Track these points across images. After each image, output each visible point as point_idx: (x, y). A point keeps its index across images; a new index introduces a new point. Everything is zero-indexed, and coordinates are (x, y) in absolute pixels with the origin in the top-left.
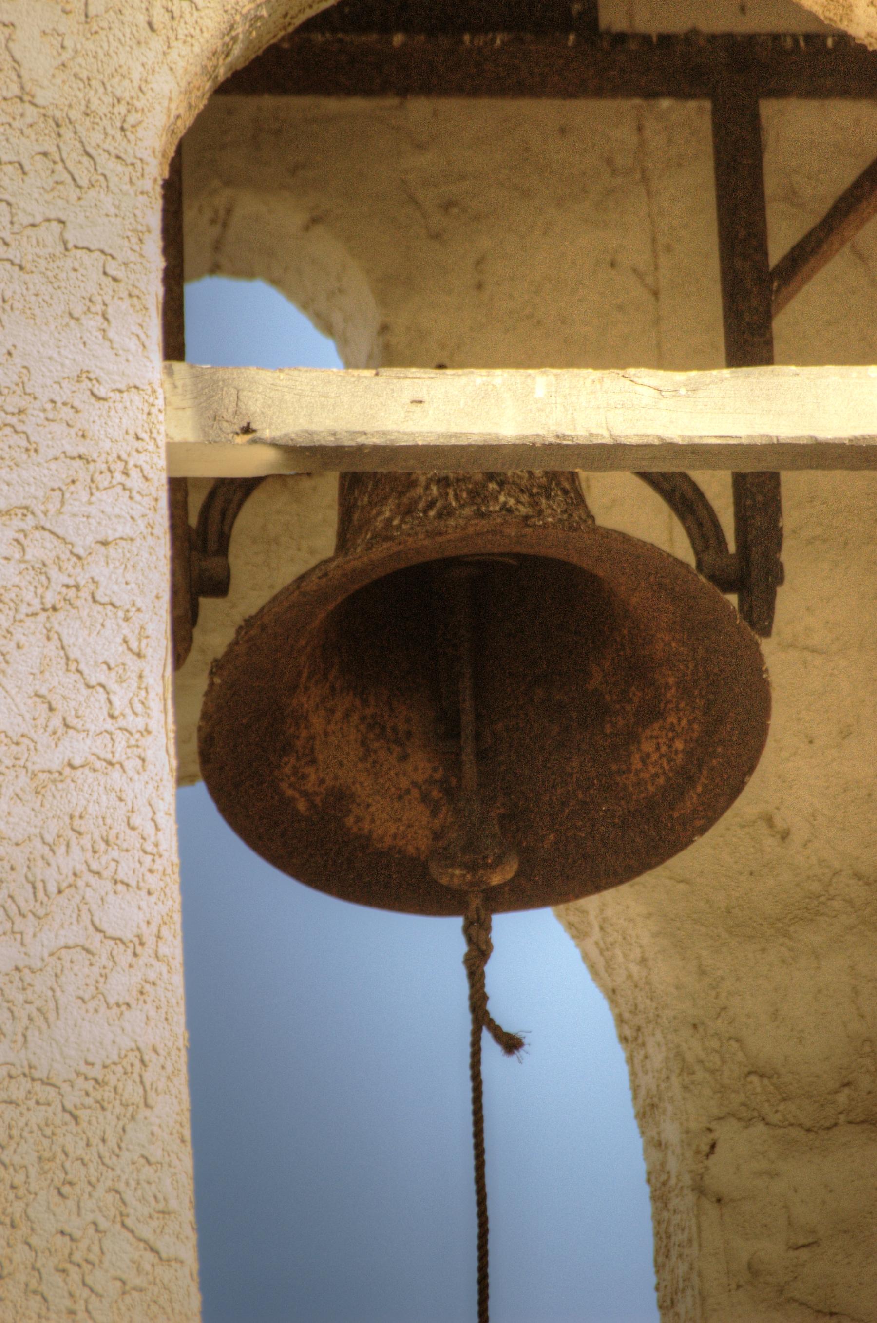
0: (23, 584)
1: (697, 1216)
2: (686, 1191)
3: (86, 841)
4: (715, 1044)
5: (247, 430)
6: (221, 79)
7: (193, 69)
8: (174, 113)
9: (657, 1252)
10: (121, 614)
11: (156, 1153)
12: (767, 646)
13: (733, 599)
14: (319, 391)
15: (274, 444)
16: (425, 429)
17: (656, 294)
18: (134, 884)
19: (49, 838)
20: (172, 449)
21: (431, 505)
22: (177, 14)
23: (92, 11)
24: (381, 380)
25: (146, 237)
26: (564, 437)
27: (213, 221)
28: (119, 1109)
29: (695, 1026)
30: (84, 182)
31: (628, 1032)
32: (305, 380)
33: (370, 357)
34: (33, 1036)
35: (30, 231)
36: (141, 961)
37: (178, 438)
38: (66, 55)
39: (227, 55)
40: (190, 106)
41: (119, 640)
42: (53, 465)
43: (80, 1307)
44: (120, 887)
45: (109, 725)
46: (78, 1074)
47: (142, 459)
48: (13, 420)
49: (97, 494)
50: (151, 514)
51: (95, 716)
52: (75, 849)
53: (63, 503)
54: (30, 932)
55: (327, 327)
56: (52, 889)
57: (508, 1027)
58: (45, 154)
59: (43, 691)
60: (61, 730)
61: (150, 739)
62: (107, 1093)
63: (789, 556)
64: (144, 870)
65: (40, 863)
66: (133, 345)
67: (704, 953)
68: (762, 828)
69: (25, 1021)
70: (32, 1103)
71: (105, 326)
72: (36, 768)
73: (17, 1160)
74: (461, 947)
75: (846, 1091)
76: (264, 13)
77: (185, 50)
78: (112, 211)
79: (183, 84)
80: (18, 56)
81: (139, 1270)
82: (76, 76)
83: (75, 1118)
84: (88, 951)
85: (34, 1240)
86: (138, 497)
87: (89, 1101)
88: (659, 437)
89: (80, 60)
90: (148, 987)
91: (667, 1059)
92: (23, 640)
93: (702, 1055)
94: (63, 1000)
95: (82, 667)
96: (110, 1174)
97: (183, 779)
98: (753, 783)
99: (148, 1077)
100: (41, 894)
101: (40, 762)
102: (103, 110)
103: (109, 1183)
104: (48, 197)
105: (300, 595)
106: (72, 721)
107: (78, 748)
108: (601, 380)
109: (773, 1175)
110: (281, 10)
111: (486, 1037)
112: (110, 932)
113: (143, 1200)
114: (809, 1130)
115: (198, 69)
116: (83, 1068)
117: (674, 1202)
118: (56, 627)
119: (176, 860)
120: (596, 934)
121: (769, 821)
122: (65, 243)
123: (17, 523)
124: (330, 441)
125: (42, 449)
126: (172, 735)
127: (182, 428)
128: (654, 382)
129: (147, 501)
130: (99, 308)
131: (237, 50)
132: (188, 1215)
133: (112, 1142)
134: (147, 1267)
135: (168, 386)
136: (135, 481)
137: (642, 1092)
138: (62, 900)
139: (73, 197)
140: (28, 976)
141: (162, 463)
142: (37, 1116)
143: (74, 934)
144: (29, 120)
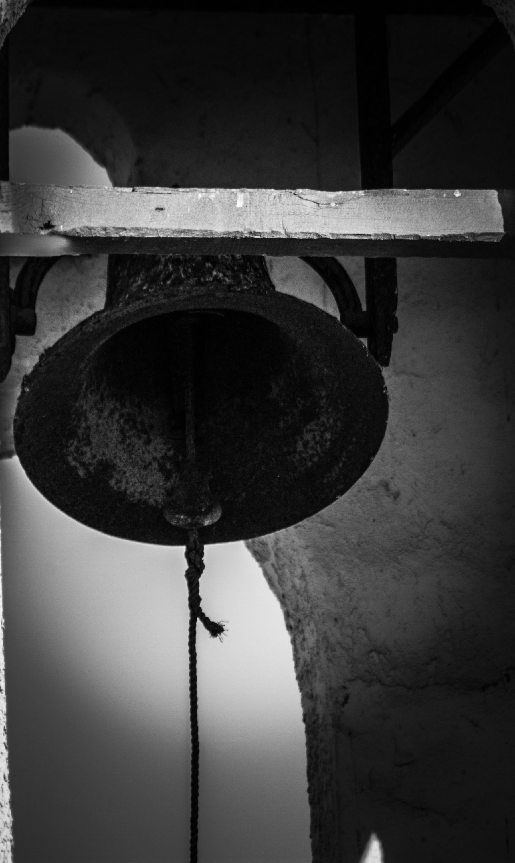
13: (364, 341)
15: (65, 235)
24: (136, 194)
26: (255, 233)
29: (336, 620)
31: (292, 623)
57: (213, 619)
63: (400, 314)
67: (343, 572)
68: (382, 490)
91: (317, 641)
108: (280, 196)
111: (199, 623)
120: (272, 559)
121: (386, 485)
124: (102, 234)
128: (314, 198)
137: (301, 662)
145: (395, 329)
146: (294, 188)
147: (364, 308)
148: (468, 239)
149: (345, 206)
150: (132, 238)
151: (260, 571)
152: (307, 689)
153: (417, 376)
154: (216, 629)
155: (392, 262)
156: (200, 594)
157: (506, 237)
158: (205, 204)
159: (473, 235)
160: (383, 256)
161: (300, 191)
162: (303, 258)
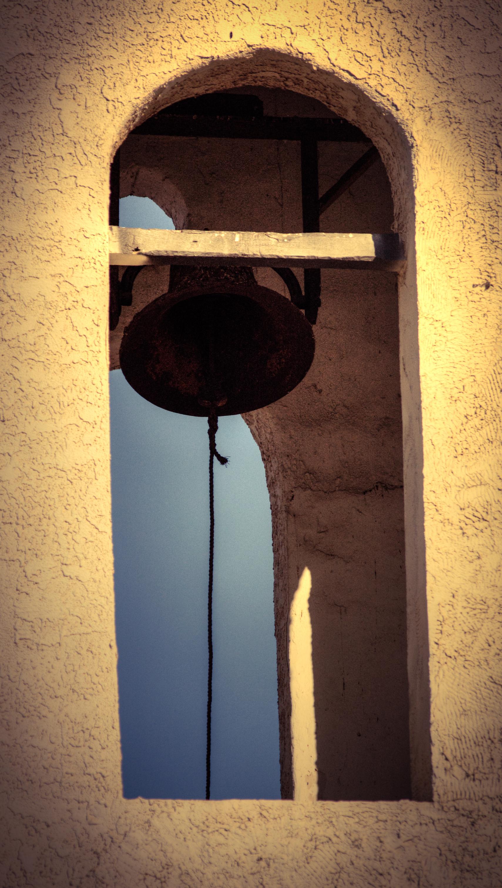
0: (59, 300)
1: (287, 521)
2: (284, 512)
3: (78, 388)
4: (295, 462)
5: (137, 250)
6: (131, 129)
7: (122, 126)
8: (115, 141)
9: (273, 532)
10: (92, 311)
11: (98, 495)
12: (314, 328)
13: (303, 311)
14: (161, 237)
15: (146, 255)
16: (197, 251)
17: (282, 205)
18: (93, 403)
19: (65, 387)
20: (111, 256)
21: (201, 277)
22: (117, 107)
23: (88, 105)
24: (183, 234)
25: (104, 183)
26: (245, 255)
27: (132, 177)
28: (86, 480)
29: (288, 456)
30: (83, 163)
31: (265, 457)
32: (156, 233)
33: (184, 225)
34: (58, 454)
35: (65, 180)
36: (95, 430)
37: (113, 252)
38: (79, 120)
39: (134, 121)
40: (121, 139)
41: (91, 320)
42: (70, 260)
43: (71, 547)
44: (89, 404)
45: (87, 349)
46: (73, 467)
47: (100, 259)
48: (57, 244)
49: (85, 270)
50: (103, 277)
51: (82, 346)
52: (74, 391)
53: (73, 273)
54: (58, 418)
55: (170, 214)
56: (66, 404)
57: (223, 455)
58: (70, 154)
59: (64, 337)
60: (70, 350)
61: (100, 354)
62: (82, 475)
63: (323, 298)
64: (97, 399)
65: (62, 395)
66: (98, 219)
67: (292, 431)
68: (312, 389)
69: (55, 449)
70: (57, 477)
71: (89, 212)
72: (61, 363)
73: (51, 496)
74: (207, 427)
75: (339, 480)
76: (147, 107)
77: (119, 119)
78: (93, 173)
79: (118, 131)
80: (62, 120)
81: (92, 535)
82: (82, 127)
83: (71, 482)
84: (77, 426)
85: (56, 524)
86: (98, 272)
87: (76, 477)
88: (278, 256)
89: (83, 122)
90: (97, 439)
91: (278, 467)
92: (58, 319)
93: (290, 466)
94: (68, 442)
95: (78, 329)
96: (83, 502)
97: (112, 368)
98: (309, 373)
99: (96, 470)
100: (62, 406)
101: (63, 361)
102: (91, 139)
103: (82, 505)
104: (71, 168)
105: (155, 307)
106: (74, 347)
107: (76, 356)
108: (258, 236)
109: (313, 507)
110: (153, 107)
111: (215, 458)
112: (85, 420)
113: (94, 511)
114: (325, 492)
115: (123, 126)
116: (75, 466)
117: (279, 515)
118: (70, 315)
119: (108, 395)
120: (255, 423)
121: (315, 386)
122: (76, 184)
123: (57, 279)
124: (165, 254)
125: (66, 254)
126: (108, 353)
127: (115, 248)
128: (276, 237)
129: (102, 273)
130: (87, 207)
131: (137, 120)
132: (109, 517)
133: (84, 491)
134: (95, 534)
135: (110, 234)
136: (98, 266)
137: (270, 479)
138: (69, 408)
139: (80, 168)
140: (56, 433)
141: (107, 259)
142: (59, 482)
143: (74, 420)
144: (65, 142)
145: (319, 305)
146: (265, 232)
147: (303, 293)
148: (356, 259)
149: (292, 241)
150: (180, 257)
151: (249, 429)
152: (272, 492)
153: (332, 329)
154: (223, 461)
155: (319, 270)
156: (422, 399)
157: (376, 259)
158: (219, 239)
159: (358, 257)
160: (314, 267)
161: (269, 233)
162: (273, 268)
